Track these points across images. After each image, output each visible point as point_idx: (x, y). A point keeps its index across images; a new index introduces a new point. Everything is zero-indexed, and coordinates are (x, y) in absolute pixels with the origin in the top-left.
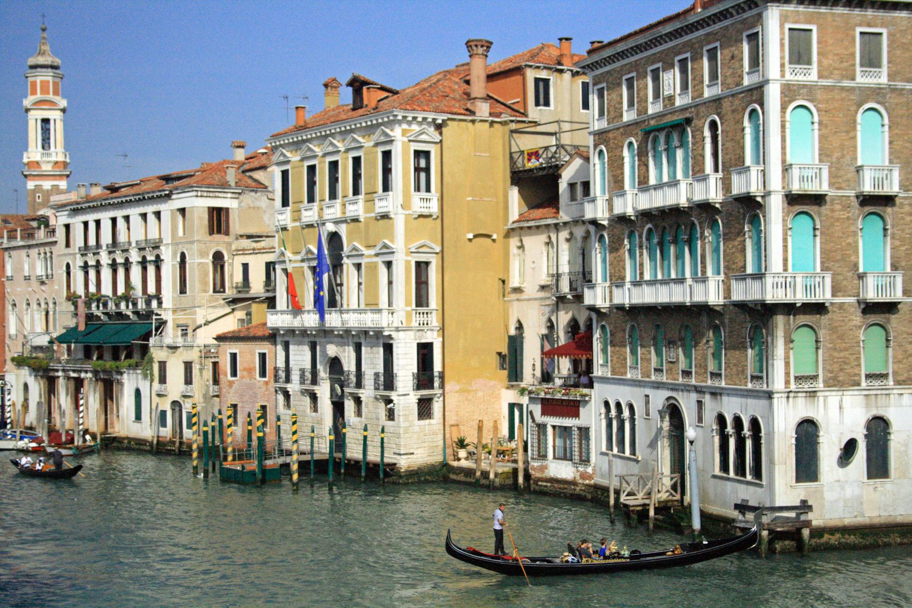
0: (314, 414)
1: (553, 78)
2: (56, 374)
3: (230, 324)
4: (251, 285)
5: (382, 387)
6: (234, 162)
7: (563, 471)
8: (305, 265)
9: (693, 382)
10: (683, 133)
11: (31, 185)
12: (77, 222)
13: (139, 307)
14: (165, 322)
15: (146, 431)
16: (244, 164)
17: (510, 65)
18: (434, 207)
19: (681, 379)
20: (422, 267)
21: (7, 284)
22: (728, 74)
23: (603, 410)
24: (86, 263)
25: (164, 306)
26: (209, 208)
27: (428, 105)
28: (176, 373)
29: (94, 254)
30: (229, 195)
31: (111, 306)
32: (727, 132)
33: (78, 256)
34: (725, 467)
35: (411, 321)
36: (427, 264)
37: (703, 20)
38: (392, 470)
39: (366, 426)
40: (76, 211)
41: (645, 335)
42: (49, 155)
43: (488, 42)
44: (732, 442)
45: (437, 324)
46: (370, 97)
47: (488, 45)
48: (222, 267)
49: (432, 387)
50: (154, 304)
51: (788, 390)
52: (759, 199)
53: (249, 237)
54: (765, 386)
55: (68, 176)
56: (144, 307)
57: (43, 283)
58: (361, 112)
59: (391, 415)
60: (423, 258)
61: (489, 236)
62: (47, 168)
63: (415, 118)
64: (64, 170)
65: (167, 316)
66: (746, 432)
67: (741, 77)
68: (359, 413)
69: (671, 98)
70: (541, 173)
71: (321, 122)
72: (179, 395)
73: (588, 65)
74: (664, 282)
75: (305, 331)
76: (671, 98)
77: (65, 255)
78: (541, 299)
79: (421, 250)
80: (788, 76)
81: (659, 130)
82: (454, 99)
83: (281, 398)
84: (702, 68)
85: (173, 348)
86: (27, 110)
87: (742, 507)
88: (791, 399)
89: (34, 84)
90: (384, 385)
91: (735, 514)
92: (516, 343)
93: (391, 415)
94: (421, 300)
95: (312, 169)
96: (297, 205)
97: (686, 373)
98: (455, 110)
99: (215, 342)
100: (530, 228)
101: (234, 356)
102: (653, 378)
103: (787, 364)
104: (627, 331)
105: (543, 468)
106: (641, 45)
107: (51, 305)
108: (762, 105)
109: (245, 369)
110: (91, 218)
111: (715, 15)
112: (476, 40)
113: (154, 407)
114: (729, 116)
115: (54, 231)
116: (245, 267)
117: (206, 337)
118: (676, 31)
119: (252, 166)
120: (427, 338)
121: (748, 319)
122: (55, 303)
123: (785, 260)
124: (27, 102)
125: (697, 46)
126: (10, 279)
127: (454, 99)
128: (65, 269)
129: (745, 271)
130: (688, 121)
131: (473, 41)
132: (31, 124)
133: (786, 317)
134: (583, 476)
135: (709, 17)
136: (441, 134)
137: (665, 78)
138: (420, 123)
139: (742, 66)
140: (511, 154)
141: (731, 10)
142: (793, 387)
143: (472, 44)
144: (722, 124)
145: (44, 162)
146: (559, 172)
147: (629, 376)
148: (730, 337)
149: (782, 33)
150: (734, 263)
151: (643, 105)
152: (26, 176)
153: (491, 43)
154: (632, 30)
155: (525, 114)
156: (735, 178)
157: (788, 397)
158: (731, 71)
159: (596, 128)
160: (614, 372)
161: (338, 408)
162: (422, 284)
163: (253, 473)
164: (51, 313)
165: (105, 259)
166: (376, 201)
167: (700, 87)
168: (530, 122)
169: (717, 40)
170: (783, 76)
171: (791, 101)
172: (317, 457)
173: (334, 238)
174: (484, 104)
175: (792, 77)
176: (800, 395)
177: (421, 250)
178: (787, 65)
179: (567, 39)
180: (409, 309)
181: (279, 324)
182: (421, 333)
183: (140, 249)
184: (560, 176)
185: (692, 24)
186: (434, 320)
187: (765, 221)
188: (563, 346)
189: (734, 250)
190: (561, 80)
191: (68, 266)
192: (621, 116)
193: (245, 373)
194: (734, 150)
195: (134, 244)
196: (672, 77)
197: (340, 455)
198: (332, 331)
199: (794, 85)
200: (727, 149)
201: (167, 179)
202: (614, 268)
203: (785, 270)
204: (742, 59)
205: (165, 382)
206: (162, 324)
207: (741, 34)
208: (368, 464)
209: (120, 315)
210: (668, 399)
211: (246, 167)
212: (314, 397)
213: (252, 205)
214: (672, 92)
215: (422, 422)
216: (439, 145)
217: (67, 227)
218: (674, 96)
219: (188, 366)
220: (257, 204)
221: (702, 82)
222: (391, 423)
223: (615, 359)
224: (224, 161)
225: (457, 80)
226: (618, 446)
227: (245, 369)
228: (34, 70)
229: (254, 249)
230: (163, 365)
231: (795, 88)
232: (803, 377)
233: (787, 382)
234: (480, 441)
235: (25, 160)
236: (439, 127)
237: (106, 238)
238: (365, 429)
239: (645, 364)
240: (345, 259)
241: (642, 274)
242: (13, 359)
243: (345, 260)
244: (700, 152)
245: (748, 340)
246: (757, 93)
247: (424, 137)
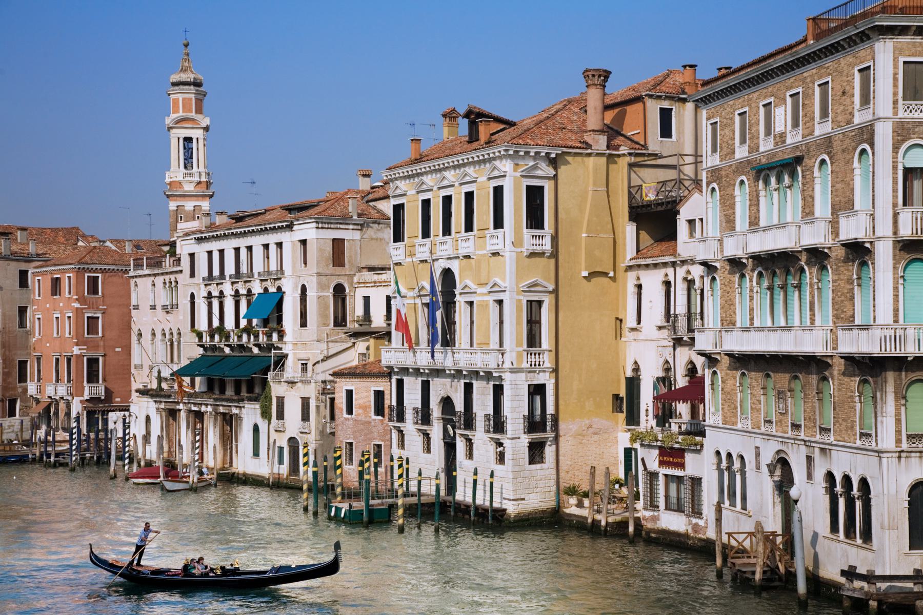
0: (427, 455)
1: (675, 108)
2: (178, 407)
3: (351, 359)
4: (372, 319)
5: (492, 430)
6: (358, 192)
7: (674, 522)
8: (418, 301)
9: (802, 436)
10: (793, 175)
11: (173, 205)
12: (201, 251)
13: (261, 340)
14: (286, 356)
15: (261, 467)
16: (369, 193)
17: (632, 94)
18: (547, 245)
19: (790, 432)
20: (534, 307)
21: (134, 312)
22: (838, 111)
23: (715, 460)
24: (210, 293)
25: (285, 339)
26: (334, 240)
27: (541, 138)
28: (293, 409)
29: (217, 284)
30: (351, 227)
31: (234, 340)
32: (837, 173)
33: (203, 286)
34: (834, 528)
35: (522, 362)
36: (540, 303)
37: (814, 52)
38: (502, 516)
39: (476, 469)
40: (200, 240)
41: (755, 384)
42: (191, 175)
43: (606, 71)
44: (842, 502)
45: (549, 365)
46: (484, 130)
47: (606, 74)
48: (344, 300)
49: (544, 431)
50: (275, 337)
51: (899, 449)
52: (868, 245)
53: (371, 269)
54: (874, 444)
55: (211, 196)
56: (265, 339)
57: (168, 312)
58: (475, 145)
59: (501, 458)
60: (535, 297)
61: (605, 274)
62: (189, 187)
63: (527, 153)
64: (207, 189)
65: (287, 349)
66: (855, 492)
67: (852, 114)
68: (470, 455)
69: (782, 136)
70: (659, 208)
71: (436, 155)
72: (298, 431)
73: (701, 99)
74: (773, 329)
75: (419, 369)
76: (782, 136)
77: (189, 285)
78: (658, 340)
79: (533, 289)
80: (901, 114)
81: (771, 168)
82: (571, 131)
83: (395, 435)
84: (813, 105)
85: (292, 383)
86: (170, 128)
87: (850, 573)
88: (903, 460)
89: (176, 102)
90: (494, 428)
91: (843, 580)
92: (633, 384)
93: (501, 458)
94: (533, 340)
95: (426, 204)
96: (412, 239)
97: (796, 426)
98: (570, 144)
99: (331, 378)
100: (647, 266)
101: (350, 393)
102: (763, 430)
103: (898, 421)
104: (738, 379)
105: (655, 519)
106: (753, 78)
107: (175, 336)
108: (872, 145)
109: (360, 407)
110: (215, 246)
111: (825, 48)
112: (594, 70)
113: (271, 441)
114: (840, 156)
115: (179, 260)
116: (367, 300)
117: (322, 372)
118: (787, 64)
119: (376, 195)
120: (540, 379)
121: (857, 372)
122: (179, 334)
123: (896, 311)
124: (168, 121)
125: (809, 80)
126: (136, 307)
127: (571, 131)
128: (189, 299)
129: (853, 321)
130: (799, 160)
131: (590, 70)
132: (174, 142)
133: (897, 373)
134: (696, 527)
135: (820, 50)
136: (556, 169)
137: (777, 113)
138: (534, 158)
139: (853, 102)
140: (630, 187)
141: (867, 32)
142: (905, 446)
143: (590, 73)
144: (832, 164)
145: (186, 182)
146: (678, 208)
147: (739, 426)
148: (839, 390)
149: (895, 67)
150: (843, 312)
151: (755, 141)
152: (168, 196)
153: (610, 73)
154: (745, 63)
155: (645, 146)
156: (843, 222)
157: (899, 457)
158: (842, 108)
159: (709, 165)
160: (725, 422)
161: (450, 448)
162: (533, 323)
163: (360, 513)
164: (175, 344)
165: (228, 290)
166: (488, 238)
167: (811, 124)
168: (650, 155)
169: (829, 74)
170: (896, 113)
171: (904, 141)
172: (424, 500)
173: (448, 274)
174: (601, 137)
175: (906, 115)
176: (913, 455)
177: (533, 289)
178: (901, 101)
179: (691, 66)
180: (521, 349)
181: (393, 363)
182: (532, 374)
183: (262, 280)
184: (678, 212)
185: (803, 57)
186: (547, 361)
187: (874, 268)
188: (680, 389)
189: (843, 298)
190: (684, 110)
191: (192, 296)
192: (734, 153)
193: (360, 411)
194: (844, 193)
195: (256, 276)
196: (783, 113)
197: (450, 498)
198: (444, 370)
199: (908, 123)
200: (837, 190)
201: (290, 209)
202: (725, 312)
203: (896, 321)
204: (853, 96)
205: (283, 419)
206: (281, 360)
207: (853, 68)
208: (477, 508)
209: (241, 347)
210: (778, 452)
211: (371, 197)
212: (427, 436)
213: (374, 237)
214: (783, 128)
215: (533, 467)
216: (553, 182)
217: (192, 256)
218: (785, 133)
219: (305, 402)
220: (380, 235)
221: (813, 119)
222: (501, 467)
223: (726, 407)
224: (349, 190)
225: (577, 110)
226: (729, 498)
227: (360, 407)
228: (176, 88)
229: (375, 282)
230: (281, 401)
231: (910, 126)
232: (917, 435)
233: (898, 441)
234: (592, 487)
235: (168, 180)
236: (554, 162)
237: (230, 269)
238: (476, 473)
239: (756, 414)
240: (458, 296)
241: (752, 319)
242: (137, 391)
243: (458, 298)
244: (810, 193)
245: (857, 394)
246: (867, 134)
247: (539, 173)
